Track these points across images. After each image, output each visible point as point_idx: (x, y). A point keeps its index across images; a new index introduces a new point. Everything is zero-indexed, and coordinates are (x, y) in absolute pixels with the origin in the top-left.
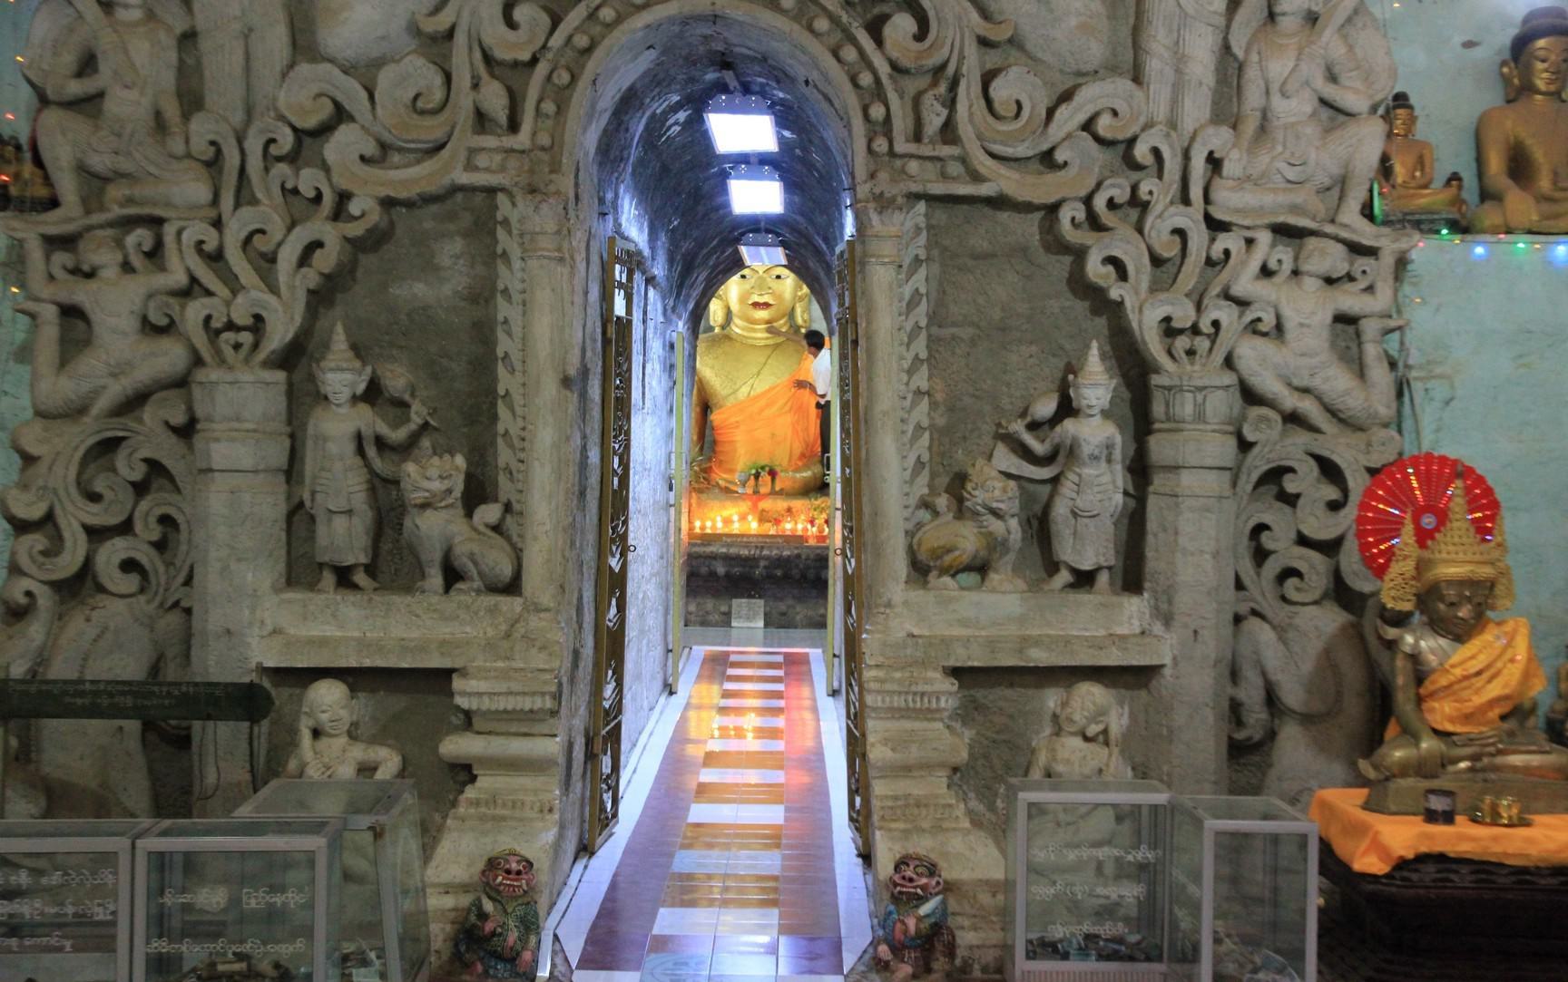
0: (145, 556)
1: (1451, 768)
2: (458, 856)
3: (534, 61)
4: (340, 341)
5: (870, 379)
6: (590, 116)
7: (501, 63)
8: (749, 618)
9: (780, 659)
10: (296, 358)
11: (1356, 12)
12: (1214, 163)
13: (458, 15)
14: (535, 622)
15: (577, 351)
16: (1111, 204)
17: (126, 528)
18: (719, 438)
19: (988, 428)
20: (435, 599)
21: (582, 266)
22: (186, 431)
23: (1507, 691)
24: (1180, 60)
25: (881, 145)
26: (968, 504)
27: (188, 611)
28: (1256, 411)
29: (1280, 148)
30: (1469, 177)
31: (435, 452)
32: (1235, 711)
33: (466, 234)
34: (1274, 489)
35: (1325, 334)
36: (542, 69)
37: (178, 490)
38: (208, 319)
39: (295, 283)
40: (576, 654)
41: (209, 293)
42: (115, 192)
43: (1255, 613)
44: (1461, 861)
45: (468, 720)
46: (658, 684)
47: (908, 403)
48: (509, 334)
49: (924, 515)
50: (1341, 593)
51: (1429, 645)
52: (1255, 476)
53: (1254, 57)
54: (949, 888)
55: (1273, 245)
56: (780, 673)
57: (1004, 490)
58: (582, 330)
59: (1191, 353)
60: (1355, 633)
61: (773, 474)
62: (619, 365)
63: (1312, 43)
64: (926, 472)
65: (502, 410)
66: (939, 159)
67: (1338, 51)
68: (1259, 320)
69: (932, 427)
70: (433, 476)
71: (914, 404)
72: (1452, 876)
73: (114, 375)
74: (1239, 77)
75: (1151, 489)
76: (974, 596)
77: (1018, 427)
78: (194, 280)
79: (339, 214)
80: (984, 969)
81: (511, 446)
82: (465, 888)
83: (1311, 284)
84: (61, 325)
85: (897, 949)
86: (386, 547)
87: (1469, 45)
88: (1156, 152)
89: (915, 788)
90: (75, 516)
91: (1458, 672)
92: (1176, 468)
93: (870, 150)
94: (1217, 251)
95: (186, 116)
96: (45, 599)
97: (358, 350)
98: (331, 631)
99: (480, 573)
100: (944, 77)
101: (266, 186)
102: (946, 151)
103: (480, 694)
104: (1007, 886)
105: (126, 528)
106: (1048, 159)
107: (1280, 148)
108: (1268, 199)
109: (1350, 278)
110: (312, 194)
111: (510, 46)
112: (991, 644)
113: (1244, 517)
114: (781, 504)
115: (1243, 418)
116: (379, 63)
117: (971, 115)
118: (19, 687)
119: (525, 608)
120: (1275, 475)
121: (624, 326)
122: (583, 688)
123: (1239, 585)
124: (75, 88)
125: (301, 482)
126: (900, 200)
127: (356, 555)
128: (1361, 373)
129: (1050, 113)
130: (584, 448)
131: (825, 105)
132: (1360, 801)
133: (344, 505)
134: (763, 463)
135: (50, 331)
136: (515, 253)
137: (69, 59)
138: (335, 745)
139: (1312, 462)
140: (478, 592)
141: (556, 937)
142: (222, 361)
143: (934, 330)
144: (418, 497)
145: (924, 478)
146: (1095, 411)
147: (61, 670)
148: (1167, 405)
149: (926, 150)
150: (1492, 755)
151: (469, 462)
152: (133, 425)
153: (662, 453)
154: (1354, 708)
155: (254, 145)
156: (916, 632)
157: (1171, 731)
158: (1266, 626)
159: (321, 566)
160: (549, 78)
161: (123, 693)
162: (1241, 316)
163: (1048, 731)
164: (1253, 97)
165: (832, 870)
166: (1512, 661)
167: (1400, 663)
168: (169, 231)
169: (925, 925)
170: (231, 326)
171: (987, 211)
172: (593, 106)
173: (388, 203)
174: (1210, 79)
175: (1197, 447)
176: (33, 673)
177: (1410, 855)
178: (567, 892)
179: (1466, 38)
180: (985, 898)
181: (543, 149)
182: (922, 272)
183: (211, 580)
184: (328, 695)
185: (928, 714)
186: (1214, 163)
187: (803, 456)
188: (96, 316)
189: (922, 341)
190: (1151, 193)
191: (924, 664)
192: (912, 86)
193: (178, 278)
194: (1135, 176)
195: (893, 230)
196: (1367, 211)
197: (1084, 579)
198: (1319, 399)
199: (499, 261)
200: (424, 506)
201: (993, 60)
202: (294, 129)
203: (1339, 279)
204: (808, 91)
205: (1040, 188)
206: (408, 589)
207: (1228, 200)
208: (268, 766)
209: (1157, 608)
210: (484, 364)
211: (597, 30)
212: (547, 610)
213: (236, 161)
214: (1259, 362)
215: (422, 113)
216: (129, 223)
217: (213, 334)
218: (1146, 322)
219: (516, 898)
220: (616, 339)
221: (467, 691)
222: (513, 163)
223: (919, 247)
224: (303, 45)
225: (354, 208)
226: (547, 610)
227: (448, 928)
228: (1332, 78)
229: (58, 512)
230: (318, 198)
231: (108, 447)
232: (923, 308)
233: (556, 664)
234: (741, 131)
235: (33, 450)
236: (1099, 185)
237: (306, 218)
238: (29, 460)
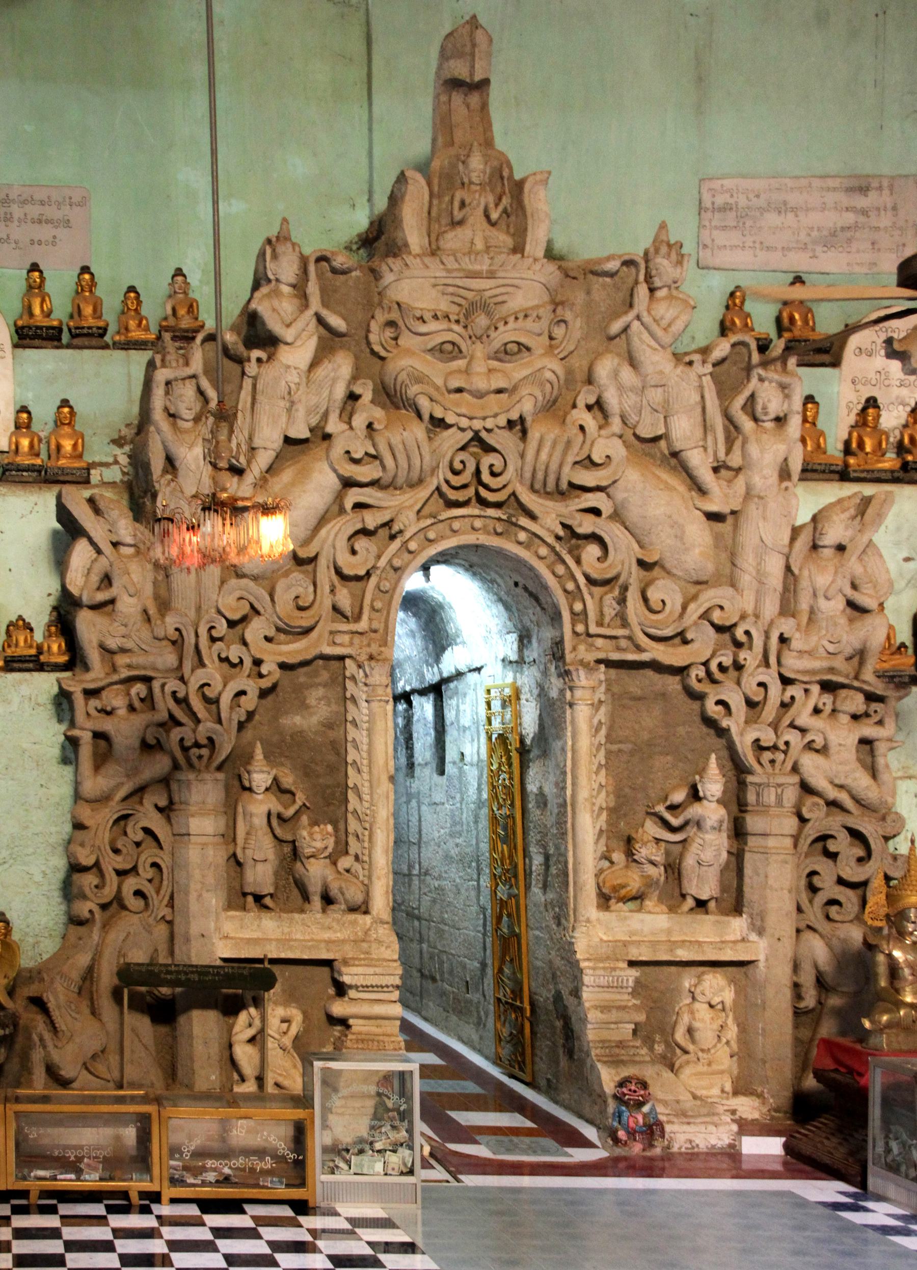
3: (368, 574)
19: (641, 810)
20: (319, 916)
28: (810, 800)
29: (824, 632)
35: (854, 751)
36: (373, 580)
37: (161, 848)
47: (595, 793)
49: (606, 864)
53: (806, 573)
63: (842, 565)
65: (351, 795)
67: (858, 570)
68: (813, 741)
70: (315, 838)
71: (599, 792)
74: (795, 585)
77: (661, 809)
78: (171, 716)
83: (845, 719)
88: (747, 633)
102: (620, 632)
105: (134, 870)
106: (682, 638)
107: (824, 632)
108: (817, 664)
109: (867, 715)
113: (802, 867)
117: (636, 608)
118: (137, 968)
123: (799, 910)
124: (101, 597)
129: (684, 608)
133: (262, 858)
137: (95, 579)
142: (191, 766)
143: (609, 746)
144: (308, 851)
145: (603, 841)
156: (605, 938)
157: (764, 1002)
158: (817, 936)
161: (192, 972)
162: (803, 737)
168: (156, 685)
170: (197, 745)
173: (283, 666)
174: (780, 588)
175: (774, 828)
179: (905, 554)
182: (603, 709)
186: (783, 640)
189: (602, 753)
193: (163, 716)
197: (701, 904)
199: (348, 702)
203: (861, 716)
207: (793, 664)
209: (753, 924)
213: (193, 641)
214: (815, 769)
216: (130, 681)
217: (185, 749)
218: (744, 741)
222: (357, 640)
225: (264, 670)
228: (854, 587)
229: (101, 861)
232: (603, 732)
237: (232, 677)
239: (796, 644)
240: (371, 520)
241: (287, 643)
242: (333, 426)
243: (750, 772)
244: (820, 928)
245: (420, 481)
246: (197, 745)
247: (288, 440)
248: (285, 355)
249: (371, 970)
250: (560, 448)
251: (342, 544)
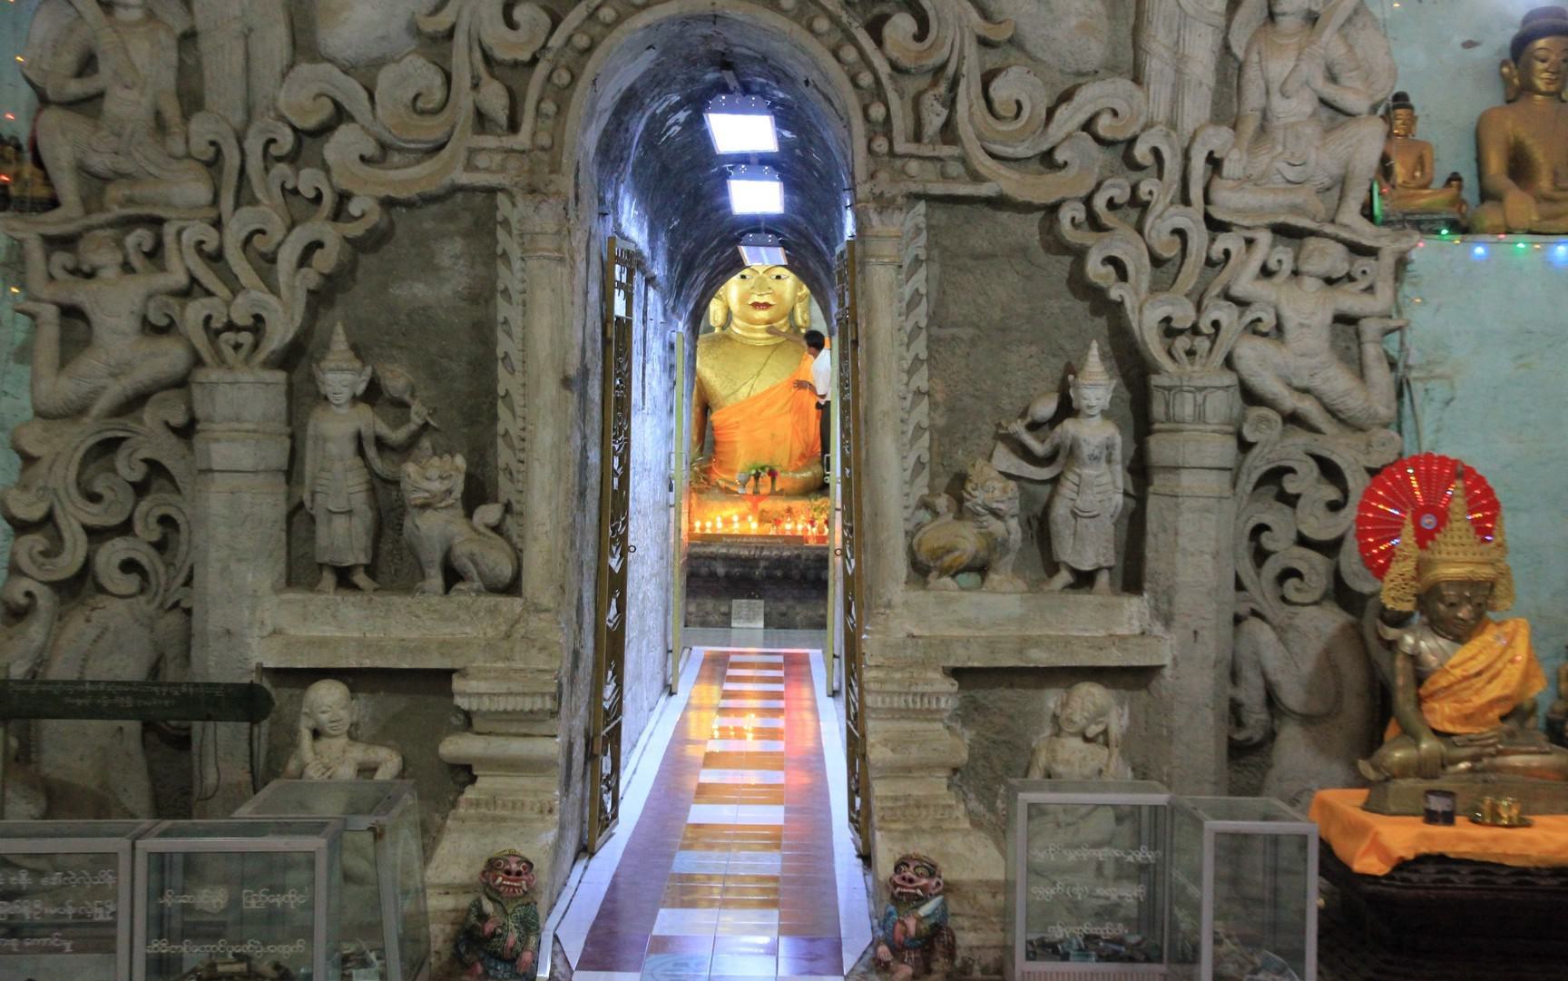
0: (145, 556)
1: (1451, 769)
2: (458, 857)
3: (534, 61)
4: (340, 341)
5: (870, 380)
6: (590, 116)
7: (501, 63)
8: (749, 618)
9: (780, 659)
10: (296, 358)
11: (1356, 12)
12: (1214, 163)
13: (458, 15)
14: (535, 623)
15: (577, 352)
16: (1111, 205)
17: (126, 528)
18: (719, 438)
19: (988, 428)
20: (435, 600)
21: (582, 267)
22: (186, 432)
23: (1507, 692)
24: (1180, 60)
25: (881, 145)
26: (968, 504)
27: (188, 612)
28: (1256, 412)
29: (1280, 149)
30: (1469, 177)
31: (435, 452)
32: (1235, 711)
33: (466, 235)
34: (1274, 490)
35: (1325, 334)
36: (542, 69)
37: (178, 491)
38: (208, 319)
39: (295, 283)
40: (576, 655)
41: (209, 293)
42: (115, 192)
43: (1255, 613)
44: (1461, 861)
45: (468, 721)
46: (658, 685)
47: (908, 403)
48: (509, 334)
49: (924, 515)
50: (1341, 594)
51: (1429, 646)
52: (1255, 477)
53: (1254, 57)
54: (949, 889)
55: (1273, 246)
56: (780, 673)
57: (1004, 491)
58: (582, 330)
59: (1191, 353)
60: (1355, 634)
61: (773, 474)
62: (619, 366)
63: (1312, 43)
64: (926, 473)
65: (502, 410)
66: (939, 159)
67: (1338, 51)
68: (1259, 320)
69: (932, 428)
70: (433, 476)
71: (914, 405)
72: (1452, 877)
73: (114, 376)
74: (1239, 77)
75: (1151, 489)
76: (974, 597)
77: (1018, 427)
78: (194, 280)
79: (339, 214)
81: (511, 447)
82: (465, 889)
83: (1311, 284)
84: (61, 326)
85: (897, 950)
86: (386, 547)
88: (1156, 152)
89: (915, 788)
90: (75, 516)
91: (1458, 672)
92: (1176, 469)
93: (870, 150)
94: (1217, 251)
95: (186, 116)
96: (45, 599)
97: (358, 350)
98: (331, 631)
99: (480, 574)
100: (944, 77)
101: (266, 186)
102: (946, 151)
103: (480, 695)
104: (1007, 887)
105: (126, 528)
106: (1048, 159)
107: (1280, 149)
108: (1268, 199)
109: (1350, 278)
110: (312, 194)
111: (510, 46)
112: (991, 645)
113: (1244, 518)
114: (781, 505)
115: (1243, 418)
116: (379, 63)
117: (971, 115)
118: (19, 688)
119: (525, 609)
120: (1275, 476)
121: (624, 326)
122: (583, 689)
123: (1239, 586)
124: (75, 88)
125: (301, 482)
126: (900, 200)
127: (356, 555)
128: (1361, 373)
129: (1050, 113)
130: (584, 449)
131: (825, 105)
132: (1360, 802)
133: (344, 506)
134: (763, 463)
135: (50, 331)
136: (515, 253)
138: (335, 745)
139: (1312, 463)
140: (478, 592)
141: (556, 938)
142: (222, 362)
143: (934, 330)
144: (418, 497)
145: (924, 479)
146: (1095, 411)
147: (61, 670)
148: (1167, 405)
149: (926, 150)
150: (1492, 756)
151: (469, 463)
152: (133, 425)
153: (662, 454)
154: (1354, 708)
155: (254, 146)
156: (916, 632)
157: (1171, 732)
158: (1266, 627)
159: (321, 566)
160: (549, 78)
161: (123, 694)
162: (1241, 316)
163: (1048, 732)
164: (1253, 97)
165: (832, 871)
166: (1512, 661)
167: (1400, 663)
168: (169, 231)
169: (925, 926)
170: (231, 326)
171: (987, 211)
172: (593, 106)
173: (388, 203)
175: (1197, 447)
176: (33, 673)
177: (1410, 856)
178: (567, 893)
179: (1466, 38)
180: (985, 899)
181: (543, 149)
182: (922, 273)
183: (211, 580)
184: (328, 695)
185: (928, 715)
186: (1214, 163)
187: (803, 456)
188: (96, 316)
189: (922, 341)
190: (1151, 193)
191: (924, 664)
192: (912, 86)
193: (178, 278)
194: (1135, 176)
195: (893, 230)
196: (1367, 212)
197: (1084, 580)
198: (1319, 399)
199: (499, 262)
200: (424, 506)
201: (993, 60)
202: (294, 129)
203: (1339, 279)
204: (808, 91)
205: (1040, 189)
206: (408, 590)
207: (1228, 200)
208: (268, 767)
209: (1157, 609)
210: (484, 364)
211: (597, 30)
212: (547, 610)
213: (236, 161)
214: (1259, 362)
215: (422, 113)
216: (129, 223)
217: (213, 334)
218: (1146, 322)
219: (516, 899)
220: (616, 339)
221: (467, 692)
222: (513, 163)
223: (919, 247)
224: (303, 45)
225: (354, 208)
226: (547, 610)
227: (448, 928)
228: (1332, 78)
229: (58, 512)
230: (318, 198)
231: (108, 447)
232: (923, 308)
233: (556, 665)
234: (741, 131)
235: (33, 450)
236: (1099, 185)
237: (306, 219)
238: (29, 460)
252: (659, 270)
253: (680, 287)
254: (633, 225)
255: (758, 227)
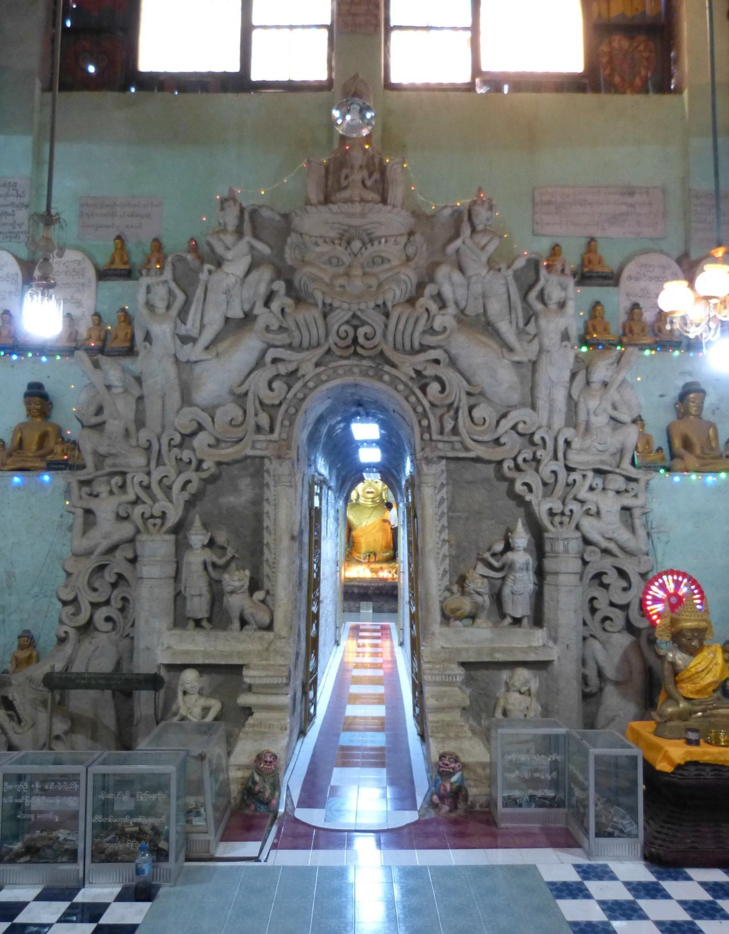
0: (115, 615)
1: (694, 716)
2: (245, 751)
3: (280, 404)
4: (197, 523)
5: (423, 536)
6: (304, 426)
7: (267, 405)
8: (367, 609)
9: (379, 627)
10: (179, 529)
12: (568, 443)
13: (250, 386)
14: (279, 644)
15: (298, 524)
16: (525, 460)
17: (107, 603)
19: (474, 555)
20: (236, 633)
21: (300, 488)
22: (133, 561)
23: (716, 679)
24: (551, 401)
25: (426, 436)
27: (132, 638)
30: (665, 447)
31: (238, 570)
33: (252, 476)
34: (597, 581)
38: (143, 514)
39: (180, 497)
40: (297, 654)
41: (144, 503)
42: (109, 461)
43: (592, 636)
44: (706, 764)
45: (250, 688)
46: (333, 642)
47: (439, 546)
48: (269, 517)
49: (447, 594)
50: (630, 628)
51: (679, 657)
52: (590, 576)
53: (582, 400)
54: (464, 766)
55: (594, 478)
56: (379, 634)
57: (482, 583)
58: (300, 515)
59: (561, 523)
60: (637, 645)
61: (375, 554)
62: (316, 527)
64: (448, 575)
65: (266, 550)
67: (617, 397)
69: (450, 556)
70: (236, 579)
71: (442, 546)
72: (703, 773)
73: (104, 538)
75: (546, 582)
76: (469, 630)
77: (487, 555)
79: (198, 468)
80: (481, 806)
81: (269, 566)
82: (247, 767)
83: (611, 494)
84: (85, 517)
85: (442, 798)
86: (216, 609)
87: (662, 396)
88: (543, 439)
89: (446, 717)
90: (86, 598)
91: (693, 670)
92: (556, 573)
93: (422, 439)
94: (570, 480)
95: (138, 430)
96: (73, 634)
97: (205, 526)
98: (191, 647)
99: (256, 622)
102: (454, 438)
103: (254, 677)
104: (491, 765)
105: (107, 603)
106: (497, 442)
109: (626, 491)
110: (188, 461)
112: (479, 651)
114: (378, 566)
115: (584, 551)
116: (216, 407)
117: (464, 424)
119: (275, 637)
120: (599, 576)
121: (318, 511)
122: (301, 667)
123: (585, 624)
124: (95, 420)
125: (181, 582)
126: (435, 459)
128: (633, 530)
129: (498, 422)
130: (301, 564)
131: (402, 420)
132: (651, 730)
133: (197, 592)
135: (80, 520)
136: (272, 483)
137: (93, 409)
138: (193, 700)
140: (255, 630)
141: (288, 786)
143: (451, 514)
144: (229, 589)
146: (521, 549)
147: (78, 667)
148: (552, 545)
149: (445, 438)
150: (711, 709)
151: (251, 572)
152: (111, 559)
153: (334, 553)
154: (638, 680)
155: (165, 441)
156: (445, 646)
159: (189, 618)
160: (286, 411)
161: (101, 678)
162: (582, 506)
163: (503, 689)
164: (582, 417)
165: (407, 743)
166: (716, 664)
167: (666, 665)
168: (129, 477)
169: (454, 787)
170: (152, 517)
171: (472, 463)
172: (305, 421)
173: (219, 464)
175: (565, 565)
176: (67, 668)
177: (682, 762)
178: (294, 758)
179: (661, 393)
180: (480, 771)
181: (284, 440)
182: (445, 490)
183: (141, 624)
184: (190, 677)
185: (451, 684)
186: (568, 443)
187: (386, 547)
188: (98, 513)
191: (449, 660)
192: (439, 412)
193: (131, 497)
194: (534, 448)
195: (432, 472)
196: (633, 463)
197: (517, 621)
198: (616, 542)
200: (232, 592)
201: (473, 401)
202: (181, 434)
204: (396, 415)
205: (495, 454)
207: (574, 458)
208: (164, 713)
210: (258, 530)
211: (307, 391)
212: (284, 638)
214: (590, 527)
215: (234, 426)
218: (542, 507)
219: (269, 774)
220: (315, 516)
221: (250, 676)
222: (271, 446)
223: (443, 479)
224: (186, 399)
225: (205, 466)
226: (284, 638)
227: (240, 787)
228: (615, 408)
230: (190, 462)
231: (102, 568)
233: (288, 662)
234: (365, 430)
235: (70, 570)
236: (519, 452)
238: (69, 575)
239: (576, 444)
240: (282, 369)
241: (227, 448)
242: (259, 309)
243: (547, 531)
244: (598, 636)
245: (319, 345)
246: (152, 517)
247: (227, 320)
248: (227, 268)
249: (264, 674)
250: (412, 321)
251: (263, 385)
252: (333, 484)
253: (341, 489)
254: (322, 467)
255: (370, 467)
